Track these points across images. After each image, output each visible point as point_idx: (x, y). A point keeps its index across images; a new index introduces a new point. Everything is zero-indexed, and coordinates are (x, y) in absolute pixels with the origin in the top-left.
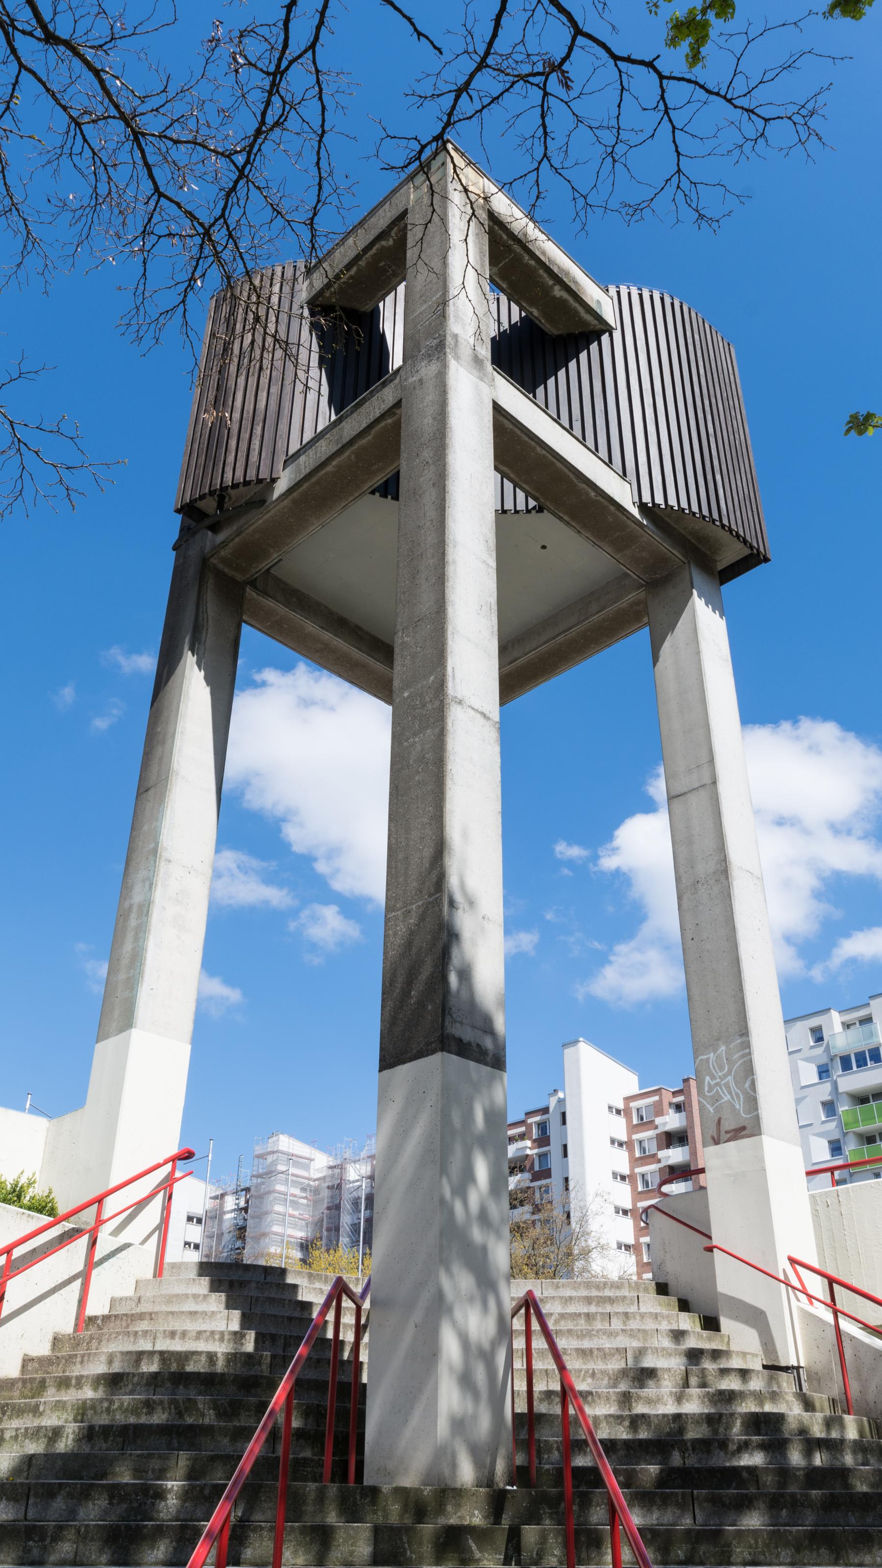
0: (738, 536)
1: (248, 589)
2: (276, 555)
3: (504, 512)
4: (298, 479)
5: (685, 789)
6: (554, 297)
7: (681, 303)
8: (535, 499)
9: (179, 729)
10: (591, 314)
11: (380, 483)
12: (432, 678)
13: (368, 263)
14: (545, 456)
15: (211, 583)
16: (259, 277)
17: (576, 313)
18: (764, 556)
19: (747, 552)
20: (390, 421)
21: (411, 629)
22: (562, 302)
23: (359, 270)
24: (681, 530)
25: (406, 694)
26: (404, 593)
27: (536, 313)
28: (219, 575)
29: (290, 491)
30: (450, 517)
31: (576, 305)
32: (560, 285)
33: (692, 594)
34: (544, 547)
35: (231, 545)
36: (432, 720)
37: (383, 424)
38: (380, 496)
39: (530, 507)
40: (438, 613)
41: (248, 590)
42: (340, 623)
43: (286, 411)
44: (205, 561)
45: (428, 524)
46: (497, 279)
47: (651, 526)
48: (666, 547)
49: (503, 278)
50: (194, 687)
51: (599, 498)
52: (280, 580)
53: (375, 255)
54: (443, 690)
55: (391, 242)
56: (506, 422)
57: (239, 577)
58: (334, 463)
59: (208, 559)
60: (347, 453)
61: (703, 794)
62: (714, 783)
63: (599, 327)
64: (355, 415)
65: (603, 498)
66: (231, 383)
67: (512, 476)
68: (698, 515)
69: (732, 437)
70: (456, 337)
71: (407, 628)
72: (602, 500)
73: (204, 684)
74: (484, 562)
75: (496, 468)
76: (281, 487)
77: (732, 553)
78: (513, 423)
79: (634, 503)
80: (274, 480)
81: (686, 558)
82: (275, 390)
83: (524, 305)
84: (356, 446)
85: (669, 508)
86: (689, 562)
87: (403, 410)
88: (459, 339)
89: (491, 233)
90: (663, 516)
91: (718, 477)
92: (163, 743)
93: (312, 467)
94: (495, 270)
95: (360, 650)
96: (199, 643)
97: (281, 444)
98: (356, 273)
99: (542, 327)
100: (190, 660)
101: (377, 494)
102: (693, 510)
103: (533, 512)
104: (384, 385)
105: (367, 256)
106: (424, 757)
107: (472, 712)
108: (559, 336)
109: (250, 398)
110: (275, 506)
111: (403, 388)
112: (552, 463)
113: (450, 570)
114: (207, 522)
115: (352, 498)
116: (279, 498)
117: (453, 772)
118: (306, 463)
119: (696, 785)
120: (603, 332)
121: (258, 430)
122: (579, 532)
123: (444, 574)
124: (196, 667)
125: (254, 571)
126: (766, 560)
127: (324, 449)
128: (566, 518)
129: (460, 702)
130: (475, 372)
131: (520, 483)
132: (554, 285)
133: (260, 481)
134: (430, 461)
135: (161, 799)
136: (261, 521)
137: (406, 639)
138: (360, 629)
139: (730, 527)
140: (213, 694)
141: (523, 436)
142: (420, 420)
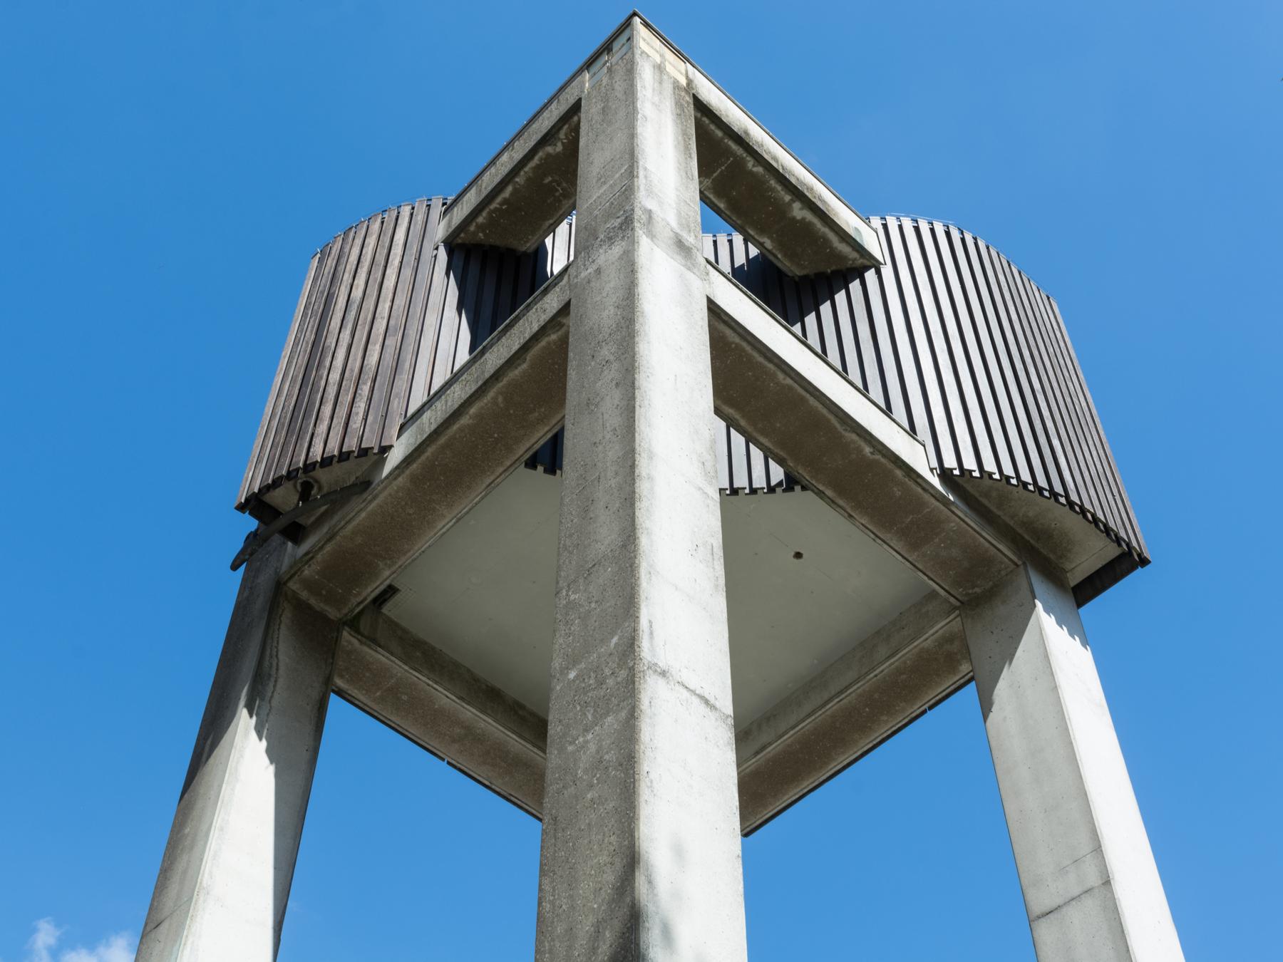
0: (1095, 520)
1: (345, 633)
2: (387, 573)
3: (735, 491)
4: (419, 441)
5: (1059, 901)
6: (794, 218)
7: (975, 239)
8: (781, 462)
9: (218, 822)
10: (848, 243)
11: (542, 442)
12: (615, 640)
13: (528, 179)
14: (790, 388)
15: (287, 616)
16: (379, 220)
17: (826, 241)
18: (1139, 555)
19: (1112, 551)
20: (554, 337)
21: (581, 581)
22: (805, 226)
23: (515, 191)
24: (1007, 520)
25: (572, 675)
26: (571, 536)
27: (768, 244)
28: (301, 607)
29: (407, 461)
30: (642, 420)
31: (826, 230)
32: (802, 202)
33: (1035, 606)
34: (798, 555)
35: (319, 557)
36: (615, 701)
37: (543, 343)
38: (546, 471)
39: (773, 483)
40: (624, 546)
41: (345, 634)
42: (489, 695)
43: (407, 365)
44: (279, 586)
45: (608, 436)
46: (711, 196)
47: (958, 503)
48: (987, 539)
49: (719, 194)
50: (248, 770)
51: (878, 457)
52: (397, 625)
53: (538, 167)
54: (634, 652)
55: (559, 148)
56: (728, 332)
57: (333, 613)
58: (473, 411)
59: (285, 583)
60: (491, 394)
61: (1090, 904)
62: (1107, 883)
63: (861, 261)
64: (504, 340)
65: (884, 456)
66: (331, 341)
67: (743, 423)
68: (1031, 488)
69: (1068, 400)
70: (649, 213)
71: (574, 581)
72: (883, 460)
73: (267, 761)
74: (700, 489)
75: (718, 412)
76: (394, 458)
77: (1089, 555)
78: (739, 334)
79: (931, 470)
80: (385, 449)
81: (1020, 558)
82: (392, 342)
83: (752, 233)
84: (505, 381)
85: (986, 476)
86: (1024, 563)
87: (571, 321)
88: (654, 216)
89: (699, 127)
90: (977, 495)
91: (1056, 442)
92: (192, 848)
93: (440, 420)
94: (708, 182)
95: (520, 736)
96: (262, 700)
97: (397, 405)
98: (511, 194)
99: (779, 265)
100: (244, 725)
101: (540, 468)
102: (1023, 478)
103: (779, 490)
104: (546, 292)
105: (526, 169)
106: (601, 762)
107: (685, 693)
108: (805, 277)
109: (356, 355)
110: (385, 488)
111: (571, 287)
112: (803, 399)
113: (643, 487)
114: (282, 522)
115: (501, 469)
116: (390, 474)
117: (652, 776)
118: (430, 421)
119: (1076, 892)
120: (867, 268)
121: (365, 389)
122: (850, 516)
123: (634, 492)
124: (254, 735)
125: (354, 601)
126: (1144, 562)
127: (458, 394)
128: (829, 493)
129: (663, 674)
130: (679, 258)
131: (755, 434)
132: (792, 201)
133: (364, 452)
134: (612, 358)
135: (177, 935)
136: (363, 515)
137: (572, 597)
138: (522, 707)
139: (1082, 507)
140: (278, 775)
141: (756, 354)
142: (599, 313)
